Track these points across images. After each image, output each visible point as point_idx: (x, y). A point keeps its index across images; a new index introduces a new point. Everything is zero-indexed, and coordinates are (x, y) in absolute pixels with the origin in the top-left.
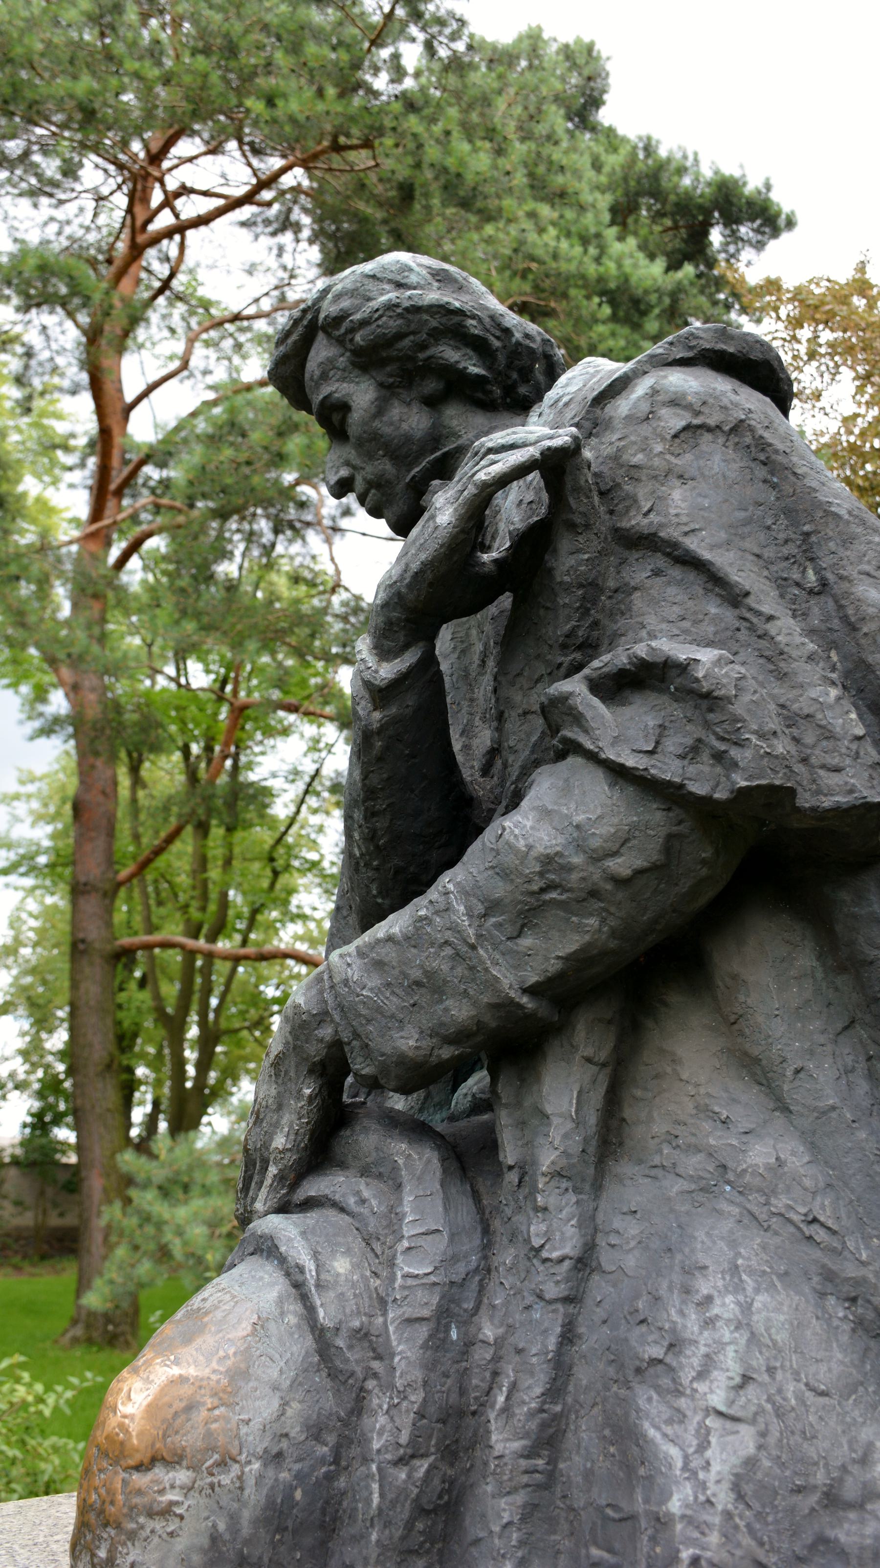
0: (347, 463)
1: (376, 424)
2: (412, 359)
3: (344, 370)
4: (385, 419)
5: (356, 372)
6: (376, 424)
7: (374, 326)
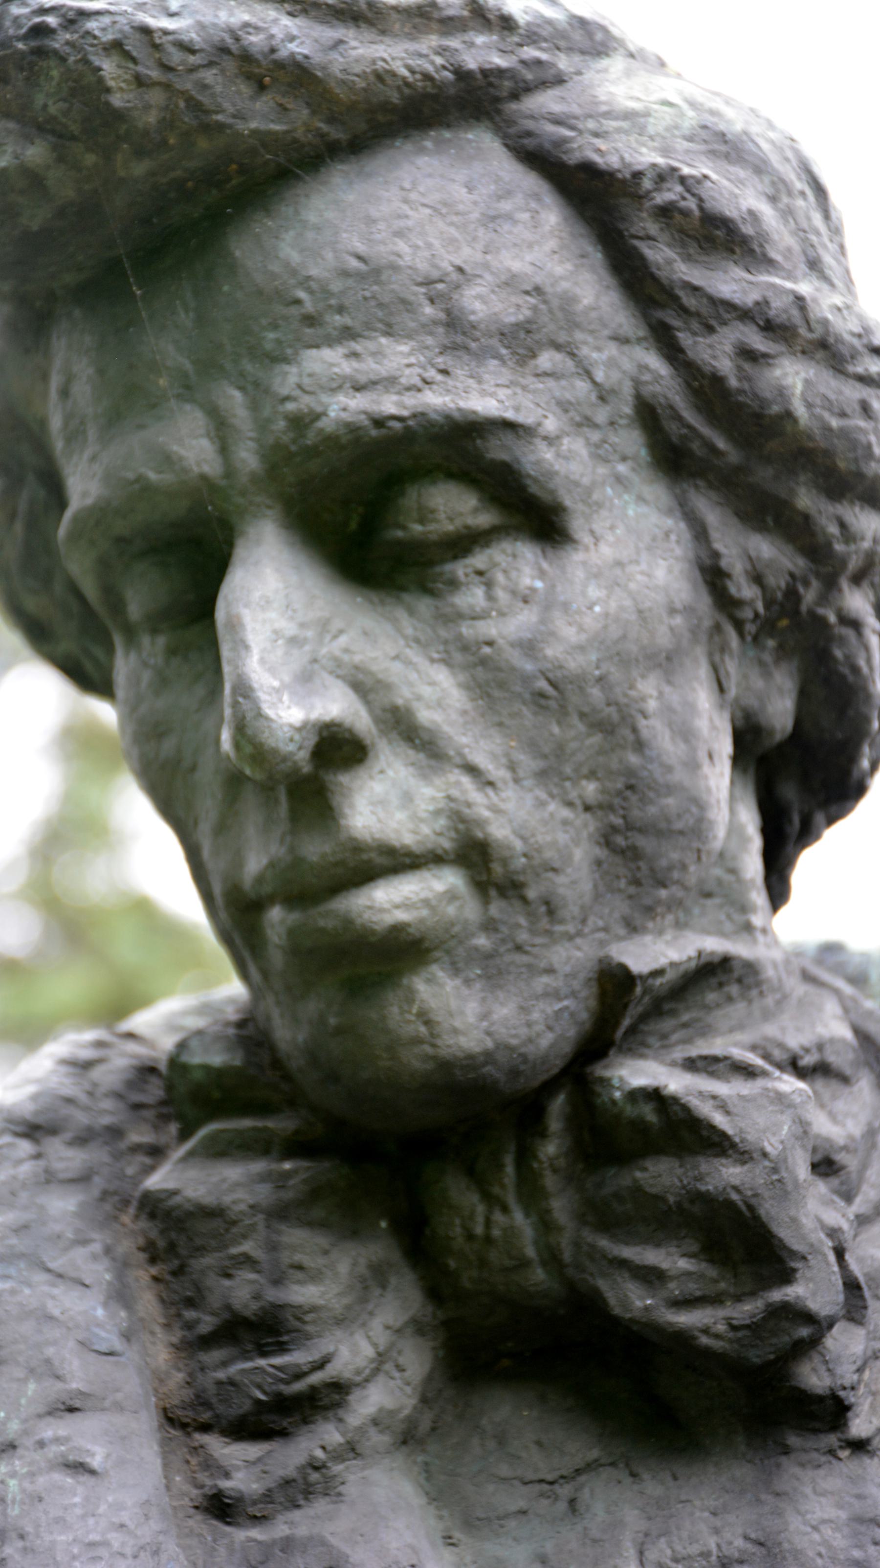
0: (362, 685)
1: (648, 688)
2: (830, 584)
3: (604, 395)
4: (673, 697)
5: (632, 441)
6: (648, 688)
7: (853, 392)
